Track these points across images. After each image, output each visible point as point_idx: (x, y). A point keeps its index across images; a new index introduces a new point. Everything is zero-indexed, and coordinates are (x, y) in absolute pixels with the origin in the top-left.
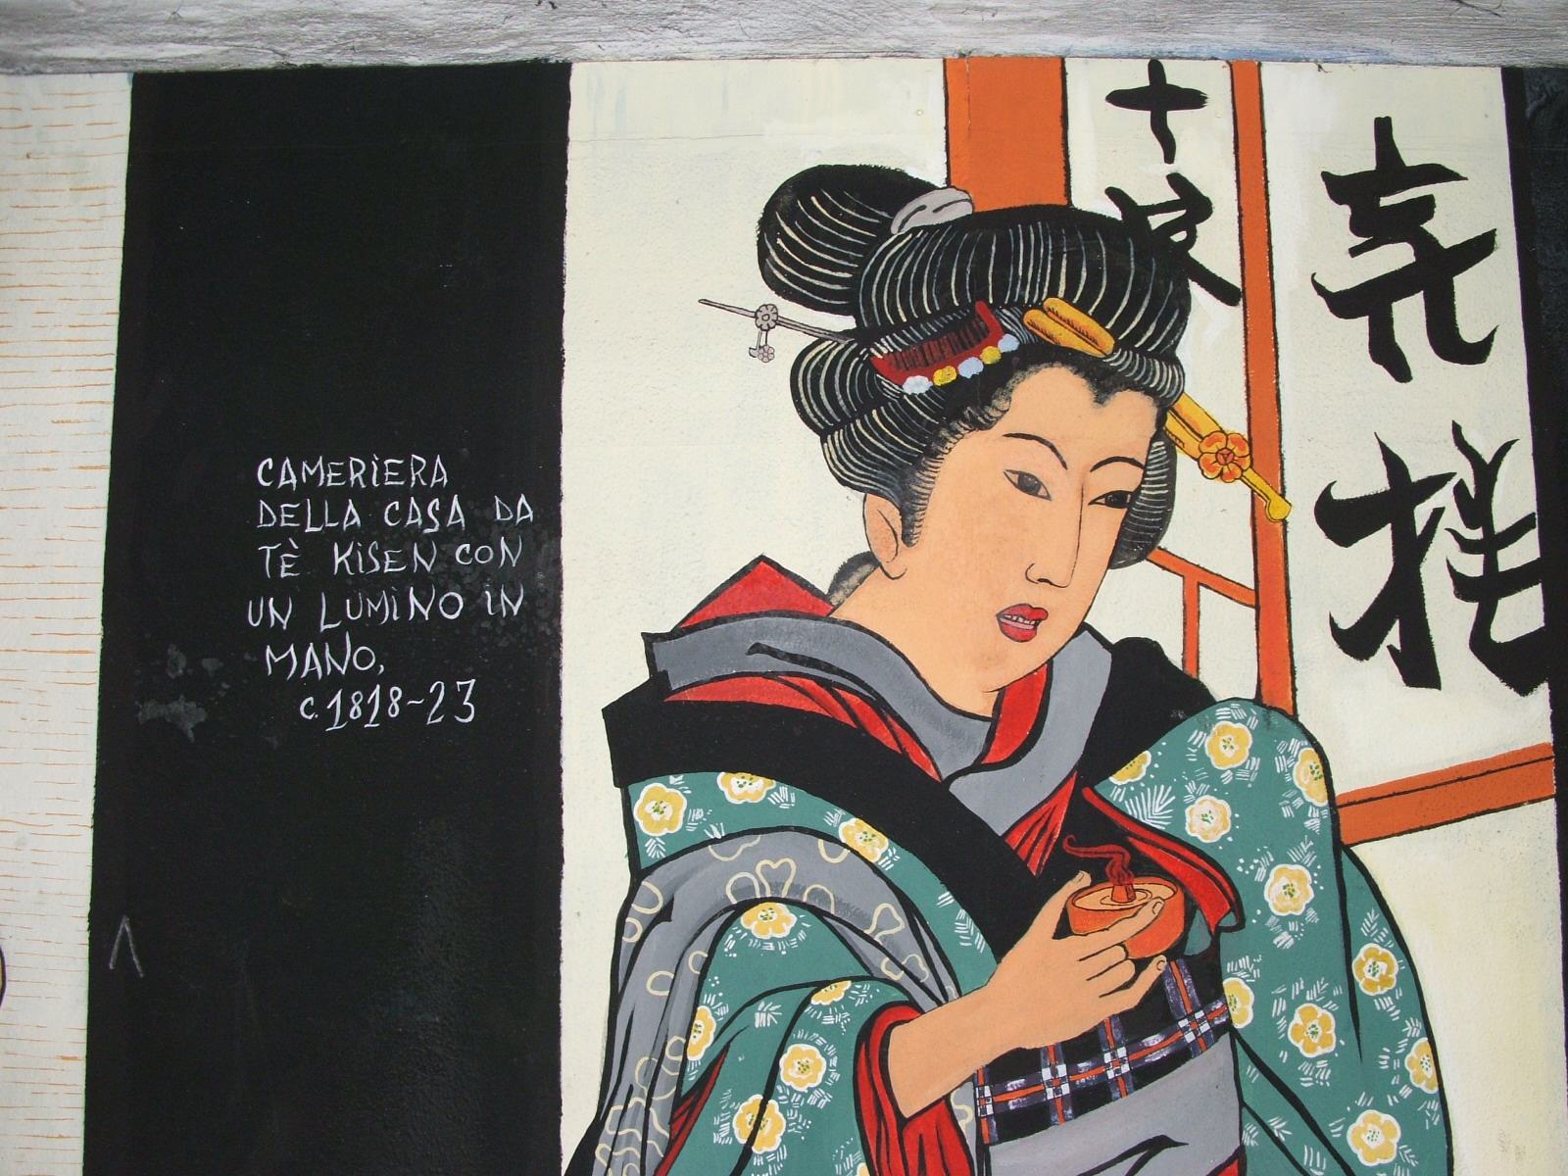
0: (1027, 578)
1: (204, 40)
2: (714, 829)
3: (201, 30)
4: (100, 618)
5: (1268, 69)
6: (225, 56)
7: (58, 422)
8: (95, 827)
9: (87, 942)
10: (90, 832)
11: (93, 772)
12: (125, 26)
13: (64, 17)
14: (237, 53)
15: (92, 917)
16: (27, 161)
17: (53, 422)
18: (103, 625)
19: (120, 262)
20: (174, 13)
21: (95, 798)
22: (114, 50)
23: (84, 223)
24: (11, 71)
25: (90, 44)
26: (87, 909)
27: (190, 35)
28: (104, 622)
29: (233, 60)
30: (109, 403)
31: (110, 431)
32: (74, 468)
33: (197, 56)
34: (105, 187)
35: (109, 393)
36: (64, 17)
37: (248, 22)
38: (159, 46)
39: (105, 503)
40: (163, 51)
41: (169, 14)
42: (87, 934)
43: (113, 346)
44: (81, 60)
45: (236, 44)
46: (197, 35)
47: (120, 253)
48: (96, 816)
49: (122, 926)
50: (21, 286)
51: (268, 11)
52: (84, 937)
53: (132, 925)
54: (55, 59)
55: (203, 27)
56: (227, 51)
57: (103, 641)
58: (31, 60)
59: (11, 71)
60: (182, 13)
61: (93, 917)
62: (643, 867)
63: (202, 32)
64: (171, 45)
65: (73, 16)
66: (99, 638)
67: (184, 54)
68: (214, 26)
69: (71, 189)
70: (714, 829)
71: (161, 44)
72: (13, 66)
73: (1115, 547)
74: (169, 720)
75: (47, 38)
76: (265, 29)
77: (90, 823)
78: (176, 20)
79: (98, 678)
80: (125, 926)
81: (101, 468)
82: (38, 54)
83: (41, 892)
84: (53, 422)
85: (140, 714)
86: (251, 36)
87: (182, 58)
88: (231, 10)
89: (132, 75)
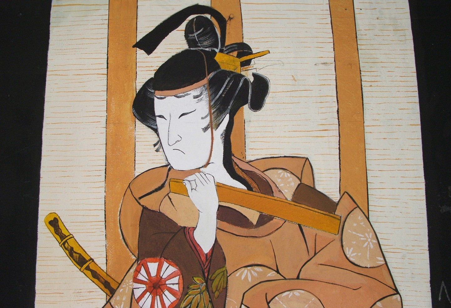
0: (197, 186)
2: (351, 250)
4: (424, 177)
5: (236, 56)
7: (401, 109)
8: (429, 250)
9: (430, 291)
10: (428, 252)
16: (377, 20)
18: (425, 179)
19: (414, 55)
21: (428, 240)
26: (429, 279)
28: (425, 178)
30: (417, 103)
31: (419, 112)
35: (417, 100)
39: (420, 137)
42: (430, 288)
47: (413, 52)
48: (429, 246)
57: (425, 185)
61: (432, 282)
62: (149, 264)
66: (424, 184)
69: (393, 30)
70: (351, 250)
81: (418, 125)
83: (412, 274)
85: (441, 210)
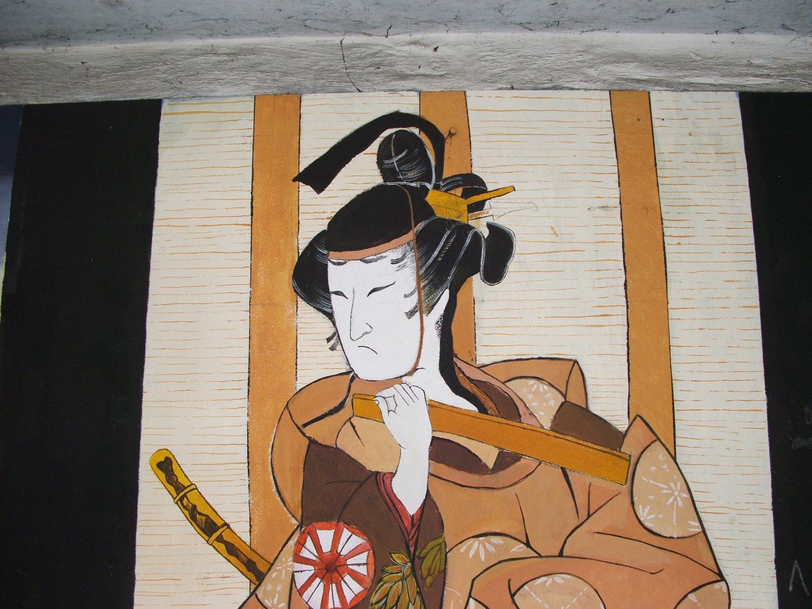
1: (768, 76)
2: (647, 510)
3: (765, 70)
6: (782, 84)
7: (728, 281)
8: (774, 510)
9: (775, 576)
10: (771, 512)
11: (770, 479)
12: (724, 67)
13: (691, 62)
14: (788, 84)
15: (777, 561)
17: (725, 281)
20: (749, 61)
22: (721, 80)
23: (726, 172)
24: (672, 89)
25: (708, 76)
26: (774, 557)
27: (760, 73)
28: (767, 394)
29: (788, 87)
30: (754, 271)
32: (739, 307)
33: (767, 84)
34: (734, 153)
36: (691, 62)
37: (789, 67)
38: (745, 78)
39: (759, 327)
40: (748, 81)
41: (746, 62)
43: (752, 240)
44: (706, 84)
45: (786, 78)
46: (763, 73)
47: (748, 189)
48: (774, 503)
49: (794, 566)
50: (696, 205)
51: (798, 62)
52: (773, 572)
53: (800, 565)
54: (692, 83)
55: (766, 69)
56: (782, 82)
57: (768, 404)
58: (680, 83)
59: (672, 89)
60: (752, 61)
62: (319, 532)
63: (766, 72)
64: (752, 78)
65: (694, 61)
66: (765, 402)
67: (760, 83)
68: (771, 69)
69: (716, 153)
70: (647, 510)
71: (747, 77)
72: (672, 87)
73: (514, 401)
74: (809, 448)
75: (685, 73)
76: (799, 71)
77: (771, 507)
78: (750, 65)
79: (767, 425)
80: (796, 565)
82: (682, 81)
83: (747, 548)
84: (725, 281)
85: (793, 445)
86: (793, 75)
87: (759, 85)
88: (778, 61)
89: (738, 93)
